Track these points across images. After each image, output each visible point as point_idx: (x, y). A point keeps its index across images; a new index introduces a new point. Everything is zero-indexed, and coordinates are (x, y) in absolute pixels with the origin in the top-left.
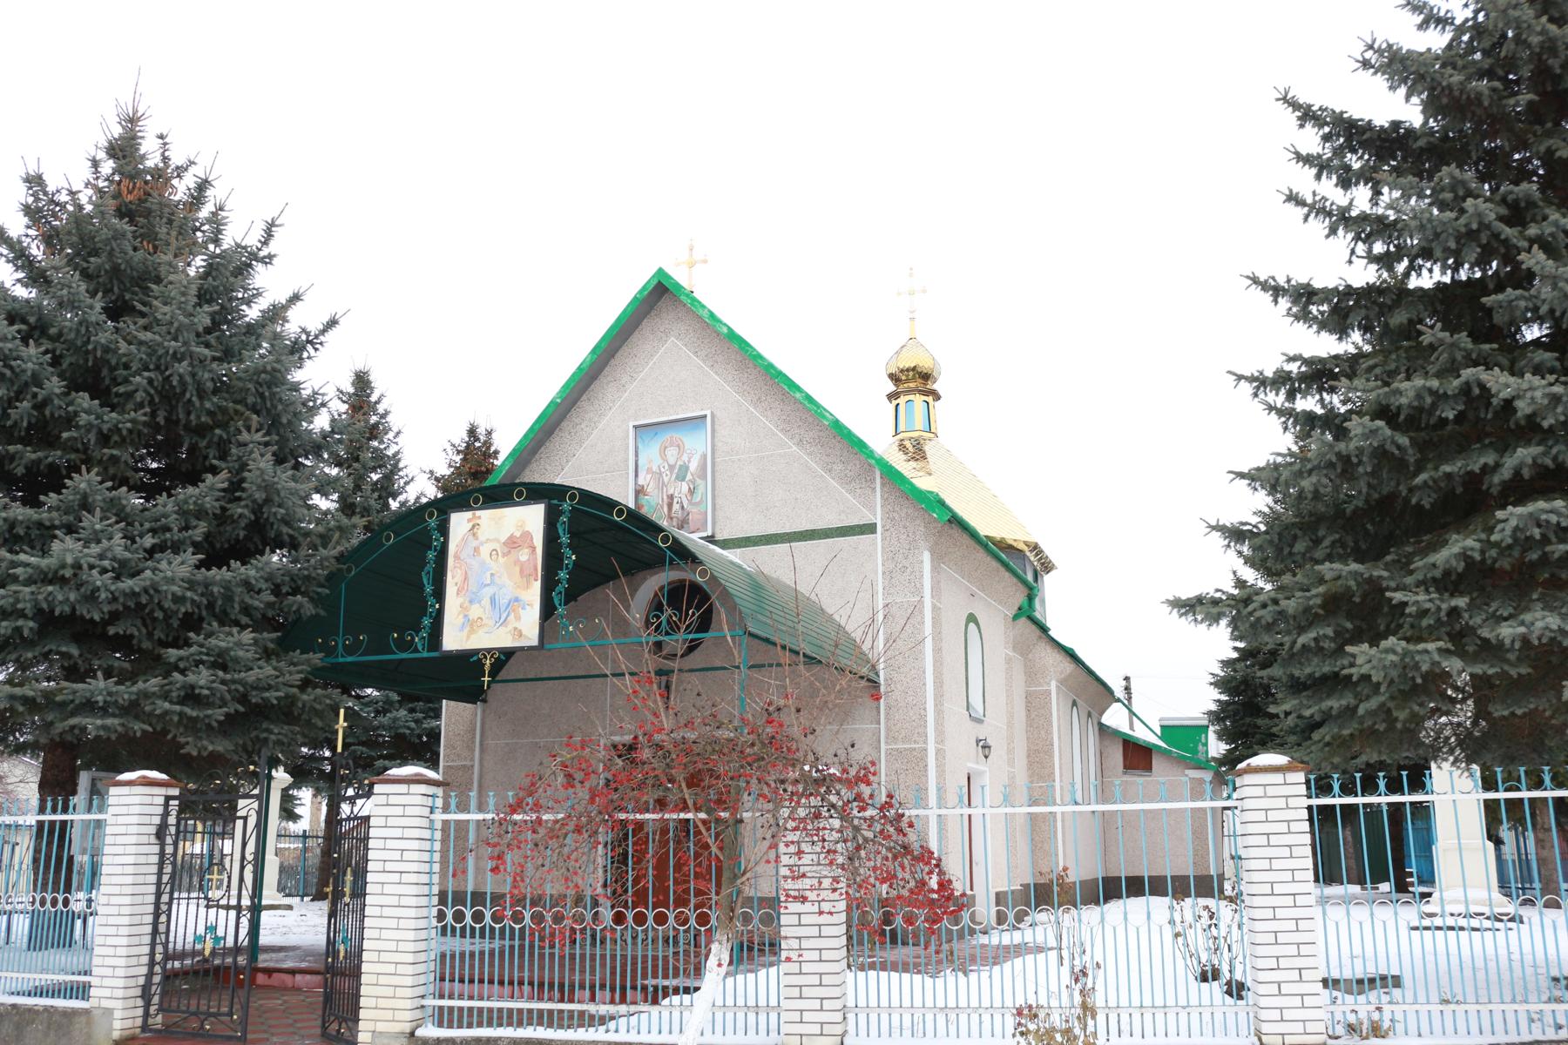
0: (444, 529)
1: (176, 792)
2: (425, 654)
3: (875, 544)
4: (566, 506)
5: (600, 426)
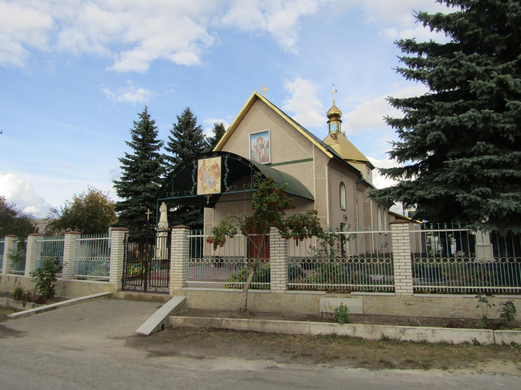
0: (197, 164)
1: (128, 232)
2: (193, 196)
3: (313, 163)
4: (226, 157)
5: (242, 135)
